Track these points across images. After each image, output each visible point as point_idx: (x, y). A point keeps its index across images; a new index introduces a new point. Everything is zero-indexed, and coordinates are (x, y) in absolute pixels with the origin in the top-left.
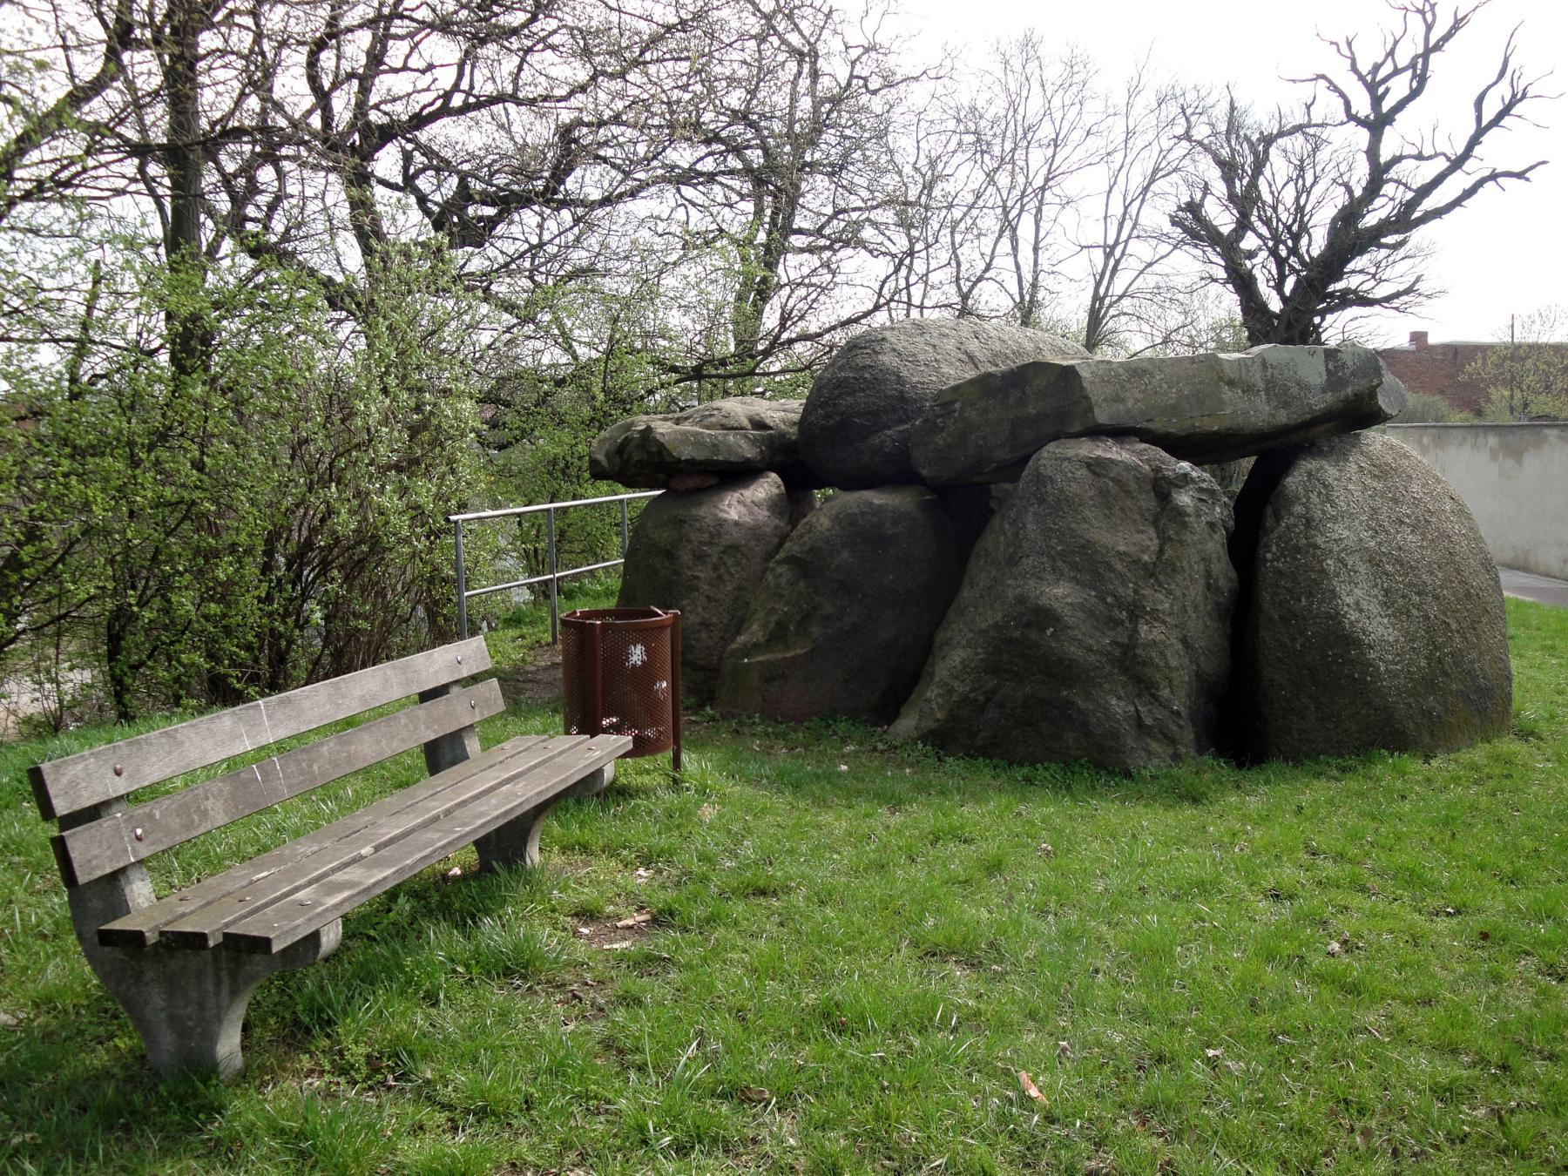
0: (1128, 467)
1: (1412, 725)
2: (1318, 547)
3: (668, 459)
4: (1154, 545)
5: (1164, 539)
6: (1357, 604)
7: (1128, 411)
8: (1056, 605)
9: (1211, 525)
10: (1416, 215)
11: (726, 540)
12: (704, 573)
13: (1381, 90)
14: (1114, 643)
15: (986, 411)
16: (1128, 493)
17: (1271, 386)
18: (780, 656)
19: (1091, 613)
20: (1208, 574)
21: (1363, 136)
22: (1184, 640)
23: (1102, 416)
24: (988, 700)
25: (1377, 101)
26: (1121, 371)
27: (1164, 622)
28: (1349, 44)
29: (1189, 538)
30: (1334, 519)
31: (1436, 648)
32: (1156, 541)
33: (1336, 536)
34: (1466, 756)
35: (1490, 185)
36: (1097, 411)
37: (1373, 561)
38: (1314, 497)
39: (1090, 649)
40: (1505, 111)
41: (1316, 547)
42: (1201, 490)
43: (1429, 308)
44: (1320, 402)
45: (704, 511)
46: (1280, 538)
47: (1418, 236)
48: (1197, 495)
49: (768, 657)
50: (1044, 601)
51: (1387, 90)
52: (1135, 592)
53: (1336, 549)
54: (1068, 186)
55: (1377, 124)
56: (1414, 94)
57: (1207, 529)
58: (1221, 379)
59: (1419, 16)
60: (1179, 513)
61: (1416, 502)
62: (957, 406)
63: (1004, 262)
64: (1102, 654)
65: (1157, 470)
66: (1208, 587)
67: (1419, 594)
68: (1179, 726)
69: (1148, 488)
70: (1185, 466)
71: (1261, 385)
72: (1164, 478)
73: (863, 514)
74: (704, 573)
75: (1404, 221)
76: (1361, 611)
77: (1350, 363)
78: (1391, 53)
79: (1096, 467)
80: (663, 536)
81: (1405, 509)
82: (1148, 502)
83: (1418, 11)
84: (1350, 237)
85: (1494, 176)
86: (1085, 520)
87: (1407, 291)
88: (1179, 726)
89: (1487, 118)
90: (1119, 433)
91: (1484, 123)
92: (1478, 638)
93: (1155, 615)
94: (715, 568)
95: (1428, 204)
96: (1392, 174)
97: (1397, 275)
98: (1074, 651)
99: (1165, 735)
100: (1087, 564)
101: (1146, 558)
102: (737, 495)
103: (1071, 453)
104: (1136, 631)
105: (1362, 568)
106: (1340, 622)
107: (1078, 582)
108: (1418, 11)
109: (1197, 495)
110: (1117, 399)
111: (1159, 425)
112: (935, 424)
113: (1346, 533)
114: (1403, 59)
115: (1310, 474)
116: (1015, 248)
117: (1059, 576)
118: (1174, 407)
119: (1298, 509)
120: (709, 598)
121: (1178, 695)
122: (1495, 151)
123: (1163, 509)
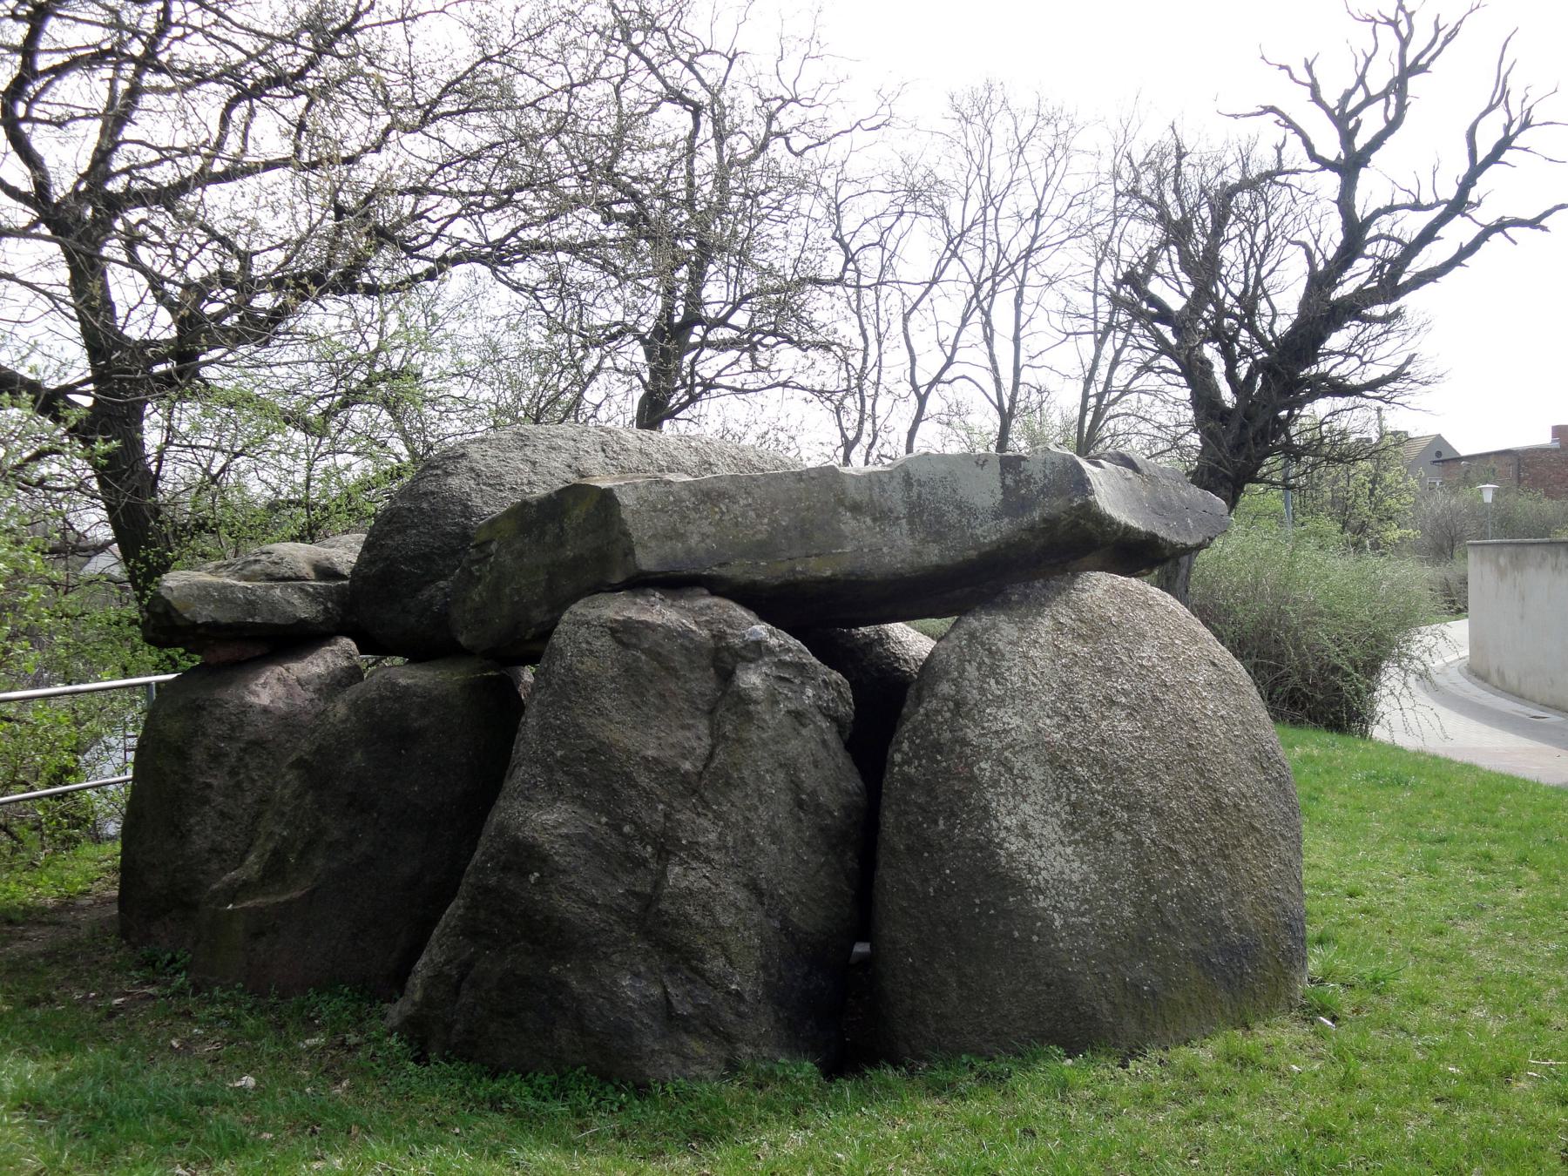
0: (669, 633)
1: (1106, 1006)
2: (967, 744)
3: (180, 623)
4: (702, 746)
5: (717, 737)
6: (1023, 826)
7: (689, 551)
8: (542, 838)
9: (798, 716)
10: (1404, 278)
11: (248, 734)
12: (218, 780)
13: (1352, 124)
14: (631, 893)
15: (521, 554)
16: (672, 672)
17: (916, 511)
18: (272, 900)
19: (597, 849)
20: (796, 786)
21: (1332, 181)
22: (753, 887)
23: (646, 560)
24: (462, 977)
25: (1347, 137)
26: (685, 494)
27: (708, 861)
28: (1309, 67)
29: (754, 736)
30: (1000, 702)
31: (1152, 890)
32: (707, 741)
33: (998, 726)
34: (1182, 1055)
35: (1497, 238)
36: (639, 552)
37: (1056, 761)
38: (971, 670)
39: (592, 903)
40: (1504, 145)
41: (965, 742)
42: (782, 664)
43: (1420, 397)
44: (990, 532)
45: (228, 695)
46: (915, 729)
47: (1409, 301)
48: (775, 672)
49: (260, 901)
50: (527, 832)
51: (1358, 123)
52: (667, 816)
53: (996, 745)
54: (1050, 262)
55: (1350, 166)
56: (1392, 126)
57: (787, 721)
58: (841, 502)
59: (1391, 29)
60: (742, 701)
61: (1144, 672)
62: (494, 547)
63: (972, 356)
64: (610, 909)
65: (719, 636)
66: (800, 804)
67: (1128, 808)
68: (740, 1015)
69: (705, 662)
70: (761, 629)
71: (902, 510)
72: (729, 648)
73: (382, 699)
74: (218, 780)
75: (1389, 285)
76: (1029, 836)
77: (1038, 476)
78: (1361, 80)
79: (624, 633)
80: (174, 728)
81: (1121, 683)
82: (703, 683)
83: (1389, 22)
84: (1323, 313)
85: (1501, 226)
86: (601, 712)
87: (1394, 377)
88: (740, 1015)
89: (1483, 152)
90: (674, 583)
91: (1480, 159)
92: (1233, 869)
93: (694, 852)
94: (233, 772)
95: (1420, 263)
96: (1372, 232)
97: (1386, 356)
98: (567, 907)
99: (715, 1030)
100: (595, 775)
101: (687, 766)
102: (279, 669)
103: (592, 614)
104: (663, 874)
105: (1037, 773)
106: (993, 855)
107: (585, 803)
108: (1389, 22)
109: (775, 672)
110: (675, 535)
111: (737, 570)
112: (471, 573)
113: (1016, 721)
114: (1377, 83)
115: (972, 636)
116: (989, 340)
117: (556, 793)
118: (761, 544)
119: (945, 688)
120: (222, 814)
121: (740, 961)
122: (1499, 193)
123: (724, 693)
